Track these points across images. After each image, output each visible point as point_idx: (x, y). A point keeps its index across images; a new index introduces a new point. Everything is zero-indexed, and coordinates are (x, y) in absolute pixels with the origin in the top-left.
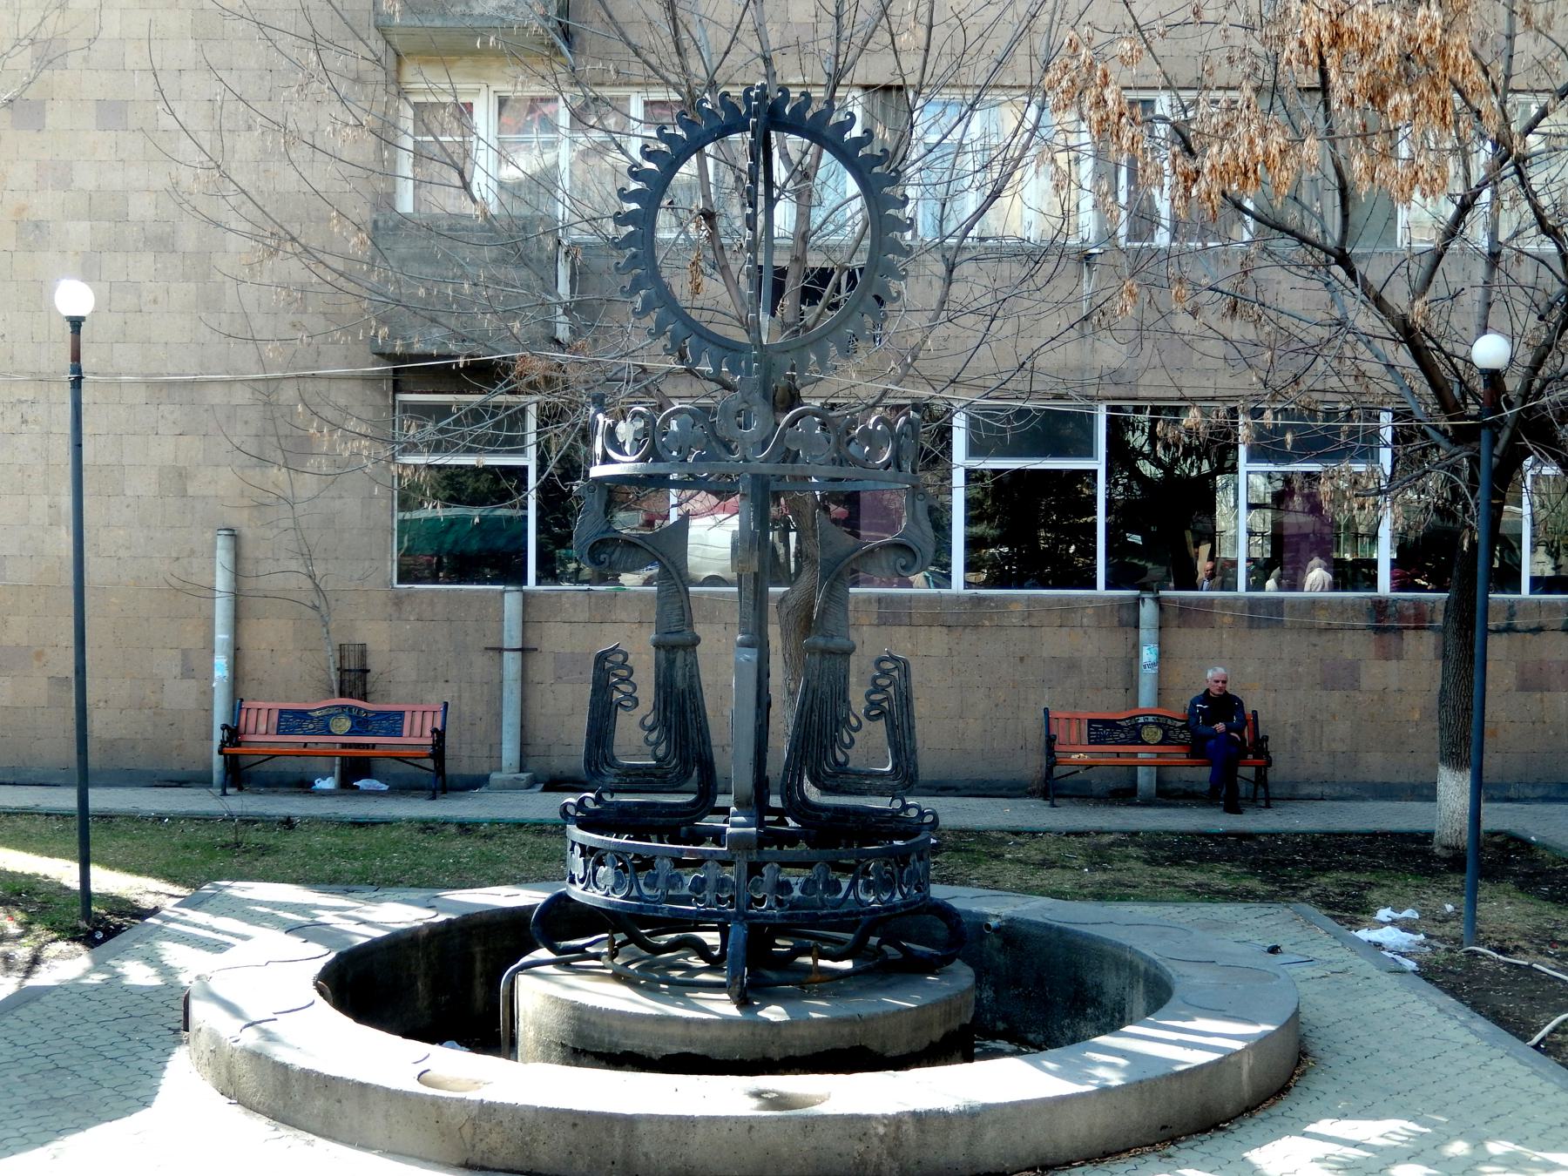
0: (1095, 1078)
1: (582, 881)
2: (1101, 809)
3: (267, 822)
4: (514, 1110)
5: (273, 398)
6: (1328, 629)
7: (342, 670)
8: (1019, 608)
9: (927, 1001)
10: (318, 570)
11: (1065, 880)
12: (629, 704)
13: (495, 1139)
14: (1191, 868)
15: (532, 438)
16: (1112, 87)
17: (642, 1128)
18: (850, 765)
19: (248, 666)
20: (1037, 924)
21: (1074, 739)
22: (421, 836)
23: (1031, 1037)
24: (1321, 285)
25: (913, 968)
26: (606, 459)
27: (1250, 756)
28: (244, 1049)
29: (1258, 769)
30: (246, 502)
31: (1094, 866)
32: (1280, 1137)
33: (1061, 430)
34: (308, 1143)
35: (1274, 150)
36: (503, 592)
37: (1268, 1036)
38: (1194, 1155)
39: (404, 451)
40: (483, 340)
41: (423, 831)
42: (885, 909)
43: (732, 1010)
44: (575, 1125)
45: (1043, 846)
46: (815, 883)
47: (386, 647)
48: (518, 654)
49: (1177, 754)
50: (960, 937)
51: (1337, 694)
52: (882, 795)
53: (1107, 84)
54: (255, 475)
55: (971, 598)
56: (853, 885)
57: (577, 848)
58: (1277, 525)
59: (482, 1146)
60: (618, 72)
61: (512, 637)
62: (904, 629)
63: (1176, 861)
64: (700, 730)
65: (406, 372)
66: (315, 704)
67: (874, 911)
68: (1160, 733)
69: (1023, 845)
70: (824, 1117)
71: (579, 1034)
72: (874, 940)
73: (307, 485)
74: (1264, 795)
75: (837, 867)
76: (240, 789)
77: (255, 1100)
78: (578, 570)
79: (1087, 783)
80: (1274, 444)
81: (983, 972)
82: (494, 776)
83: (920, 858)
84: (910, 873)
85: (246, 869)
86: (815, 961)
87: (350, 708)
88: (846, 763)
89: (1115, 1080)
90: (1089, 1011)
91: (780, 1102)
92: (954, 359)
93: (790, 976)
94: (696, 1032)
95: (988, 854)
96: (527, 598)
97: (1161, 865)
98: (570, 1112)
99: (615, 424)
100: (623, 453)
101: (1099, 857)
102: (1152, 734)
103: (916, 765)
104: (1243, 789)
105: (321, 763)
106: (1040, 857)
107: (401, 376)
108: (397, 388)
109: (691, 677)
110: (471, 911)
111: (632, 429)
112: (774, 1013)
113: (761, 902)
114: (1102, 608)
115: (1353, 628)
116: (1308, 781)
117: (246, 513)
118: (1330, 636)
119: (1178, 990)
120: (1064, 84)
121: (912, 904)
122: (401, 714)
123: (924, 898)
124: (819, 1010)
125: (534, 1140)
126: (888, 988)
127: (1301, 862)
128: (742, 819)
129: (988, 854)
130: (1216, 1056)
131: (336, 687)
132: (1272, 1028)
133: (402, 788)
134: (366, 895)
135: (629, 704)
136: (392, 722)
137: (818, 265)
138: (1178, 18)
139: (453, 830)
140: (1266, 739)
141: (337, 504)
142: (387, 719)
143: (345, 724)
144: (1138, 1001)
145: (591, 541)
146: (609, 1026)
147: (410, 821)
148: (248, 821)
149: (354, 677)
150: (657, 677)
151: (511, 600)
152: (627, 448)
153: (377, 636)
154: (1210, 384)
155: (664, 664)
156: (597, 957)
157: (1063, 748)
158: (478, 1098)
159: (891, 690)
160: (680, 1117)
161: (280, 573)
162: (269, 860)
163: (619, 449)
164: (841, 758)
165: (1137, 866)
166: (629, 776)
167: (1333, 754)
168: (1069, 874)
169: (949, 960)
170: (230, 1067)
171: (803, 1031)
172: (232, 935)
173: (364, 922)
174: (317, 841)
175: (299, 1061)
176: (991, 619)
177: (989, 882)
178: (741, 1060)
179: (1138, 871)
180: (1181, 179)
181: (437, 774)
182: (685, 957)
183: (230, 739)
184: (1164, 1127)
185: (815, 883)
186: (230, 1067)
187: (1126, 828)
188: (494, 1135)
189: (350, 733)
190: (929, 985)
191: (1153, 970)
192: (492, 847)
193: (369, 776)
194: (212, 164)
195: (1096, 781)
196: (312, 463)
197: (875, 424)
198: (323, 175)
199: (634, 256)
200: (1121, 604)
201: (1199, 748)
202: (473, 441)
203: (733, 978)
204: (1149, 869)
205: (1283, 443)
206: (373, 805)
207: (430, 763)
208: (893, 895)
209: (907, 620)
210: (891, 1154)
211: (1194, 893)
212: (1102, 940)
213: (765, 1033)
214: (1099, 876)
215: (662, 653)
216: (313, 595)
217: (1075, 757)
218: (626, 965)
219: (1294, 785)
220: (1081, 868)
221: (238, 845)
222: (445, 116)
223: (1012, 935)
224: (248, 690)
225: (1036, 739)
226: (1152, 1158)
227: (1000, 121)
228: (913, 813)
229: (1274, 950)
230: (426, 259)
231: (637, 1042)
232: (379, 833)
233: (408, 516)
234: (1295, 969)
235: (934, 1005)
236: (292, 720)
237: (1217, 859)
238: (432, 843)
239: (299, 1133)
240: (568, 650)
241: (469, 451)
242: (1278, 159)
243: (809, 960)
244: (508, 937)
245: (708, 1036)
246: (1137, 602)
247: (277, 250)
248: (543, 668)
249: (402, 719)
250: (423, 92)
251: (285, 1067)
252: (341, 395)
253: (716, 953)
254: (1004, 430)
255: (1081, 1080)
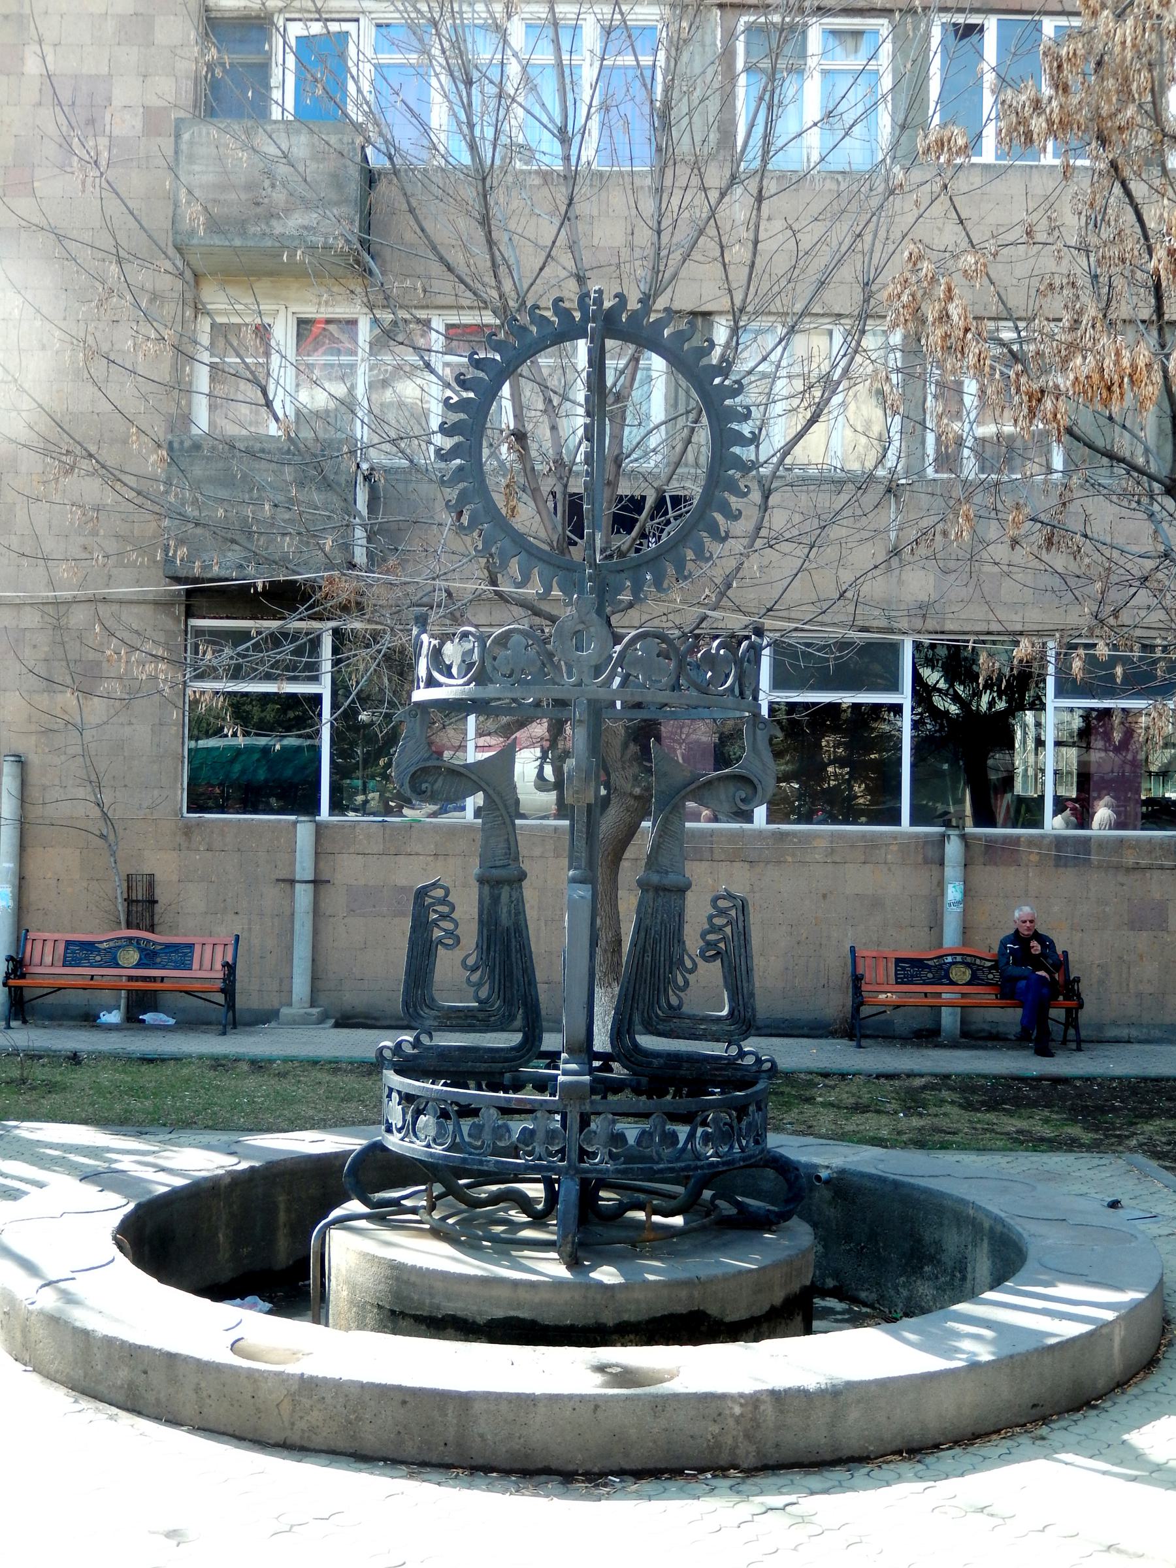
0: (962, 1351)
1: (399, 1130)
2: (909, 1050)
3: (53, 1057)
4: (337, 1386)
5: (63, 622)
6: (1137, 868)
7: (129, 901)
8: (823, 843)
9: (767, 1262)
10: (107, 799)
11: (882, 1126)
12: (450, 942)
13: (316, 1417)
14: (1010, 1114)
15: (327, 666)
16: (957, 301)
17: (478, 1407)
18: (685, 1009)
19: (34, 896)
20: (870, 1177)
21: (882, 978)
22: (212, 1074)
23: (863, 1295)
24: (1146, 516)
25: (749, 1224)
26: (431, 682)
27: (1061, 998)
28: (41, 1312)
29: (1069, 1011)
30: (33, 728)
31: (909, 1111)
32: (1158, 1417)
33: (871, 662)
34: (111, 1417)
35: (1141, 363)
36: (295, 823)
37: (1137, 1306)
38: (1069, 1437)
39: (200, 677)
40: (283, 562)
41: (214, 1068)
42: (724, 1164)
43: (560, 1271)
44: (404, 1403)
45: (854, 1089)
46: (651, 1134)
47: (175, 878)
48: (311, 886)
49: (986, 995)
50: (794, 1188)
51: (1145, 934)
52: (718, 1040)
53: (950, 298)
54: (43, 701)
55: (774, 833)
56: (691, 1136)
57: (395, 1095)
58: (1083, 765)
59: (301, 1425)
60: (425, 291)
61: (304, 867)
62: (705, 864)
63: (993, 1105)
64: (525, 971)
65: (201, 596)
66: (102, 935)
67: (712, 1164)
68: (968, 972)
69: (833, 1087)
70: (676, 1397)
71: (397, 1295)
72: (707, 1194)
73: (97, 709)
74: (1077, 1039)
75: (675, 1118)
76: (25, 1022)
77: (53, 1368)
78: (366, 802)
79: (889, 1023)
80: (1100, 678)
81: (825, 1234)
82: (284, 1011)
83: (759, 1109)
84: (749, 1124)
85: (33, 1108)
86: (648, 1217)
87: (138, 940)
88: (680, 1007)
89: (985, 1354)
90: (926, 1269)
91: (626, 1377)
92: (777, 584)
93: (623, 1234)
94: (522, 1294)
95: (799, 1097)
96: (320, 828)
97: (978, 1110)
98: (399, 1388)
99: (442, 644)
100: (451, 676)
101: (913, 1101)
102: (961, 974)
103: (754, 1009)
104: (1056, 1030)
105: (106, 996)
106: (852, 1100)
107: (193, 601)
108: (189, 613)
109: (517, 914)
110: (275, 1158)
111: (460, 651)
112: (607, 1275)
113: (594, 1155)
114: (908, 845)
115: (1162, 868)
116: (1114, 1023)
117: (33, 738)
118: (1138, 875)
119: (1032, 1252)
120: (905, 298)
121: (751, 1157)
122: (191, 946)
123: (762, 1151)
124: (655, 1271)
125: (359, 1419)
126: (724, 1247)
127: (1121, 1109)
128: (574, 1066)
129: (799, 1097)
130: (1085, 1328)
131: (123, 918)
132: (1141, 1296)
133: (189, 1023)
134: (160, 1138)
135: (450, 942)
136: (181, 954)
137: (628, 493)
138: (1010, 237)
139: (245, 1067)
140: (1077, 980)
141: (127, 730)
142: (176, 952)
143: (134, 956)
144: (982, 1265)
145: (413, 769)
146: (431, 1287)
147: (200, 1057)
148: (33, 1056)
149: (141, 905)
150: (480, 915)
151: (304, 830)
152: (454, 671)
153: (162, 864)
154: (1018, 618)
155: (487, 901)
156: (414, 1210)
157: (869, 988)
158: (299, 1372)
159: (728, 930)
160: (518, 1395)
161: (67, 800)
162: (56, 1098)
163: (447, 671)
164: (674, 1001)
165: (955, 1111)
166: (449, 1018)
167: (1139, 995)
168: (884, 1120)
169: (785, 1216)
170: (25, 1331)
171: (638, 1295)
172: (21, 1180)
173: (163, 1170)
174: (105, 1077)
175: (102, 1327)
176: (793, 855)
177: (803, 1127)
178: (572, 1326)
179: (955, 1117)
180: (1026, 398)
181: (228, 1009)
182: (506, 1210)
183: (14, 971)
184: (1034, 1406)
185: (651, 1134)
186: (25, 1331)
187: (938, 1070)
188: (315, 1413)
189: (139, 965)
190: (768, 1244)
191: (999, 1228)
192: (286, 1085)
193: (155, 1009)
194: (10, 378)
195: (899, 1021)
196: (104, 687)
197: (719, 648)
198: (125, 392)
199: (460, 468)
200: (926, 840)
201: (1007, 990)
202: (272, 667)
203: (564, 1236)
204: (966, 1115)
205: (1113, 676)
206: (161, 1040)
207: (220, 998)
208: (732, 1147)
209: (707, 855)
210: (748, 1436)
211: (1016, 1140)
212: (942, 1195)
213: (599, 1297)
214: (916, 1122)
215: (486, 888)
216: (102, 823)
217: (882, 996)
218: (444, 1219)
219: (1100, 1027)
220: (896, 1113)
221: (23, 1081)
222: (249, 336)
223: (844, 1187)
224: (33, 920)
225: (839, 975)
226: (1024, 1440)
227: (820, 347)
228: (749, 1060)
229: (1114, 1205)
230: (227, 480)
231: (460, 1304)
232: (169, 1070)
233: (202, 743)
234: (1141, 1226)
235: (775, 1265)
236: (79, 951)
237: (1034, 1104)
238: (225, 1081)
239: (101, 1405)
240: (362, 882)
241: (268, 677)
242: (1144, 372)
243: (641, 1215)
244: (315, 1189)
245: (537, 1300)
246: (943, 838)
247: (72, 468)
248: (336, 900)
249: (192, 952)
250: (225, 313)
251: (86, 1334)
252: (133, 617)
253: (540, 1207)
254: (827, 660)
255: (950, 1353)
